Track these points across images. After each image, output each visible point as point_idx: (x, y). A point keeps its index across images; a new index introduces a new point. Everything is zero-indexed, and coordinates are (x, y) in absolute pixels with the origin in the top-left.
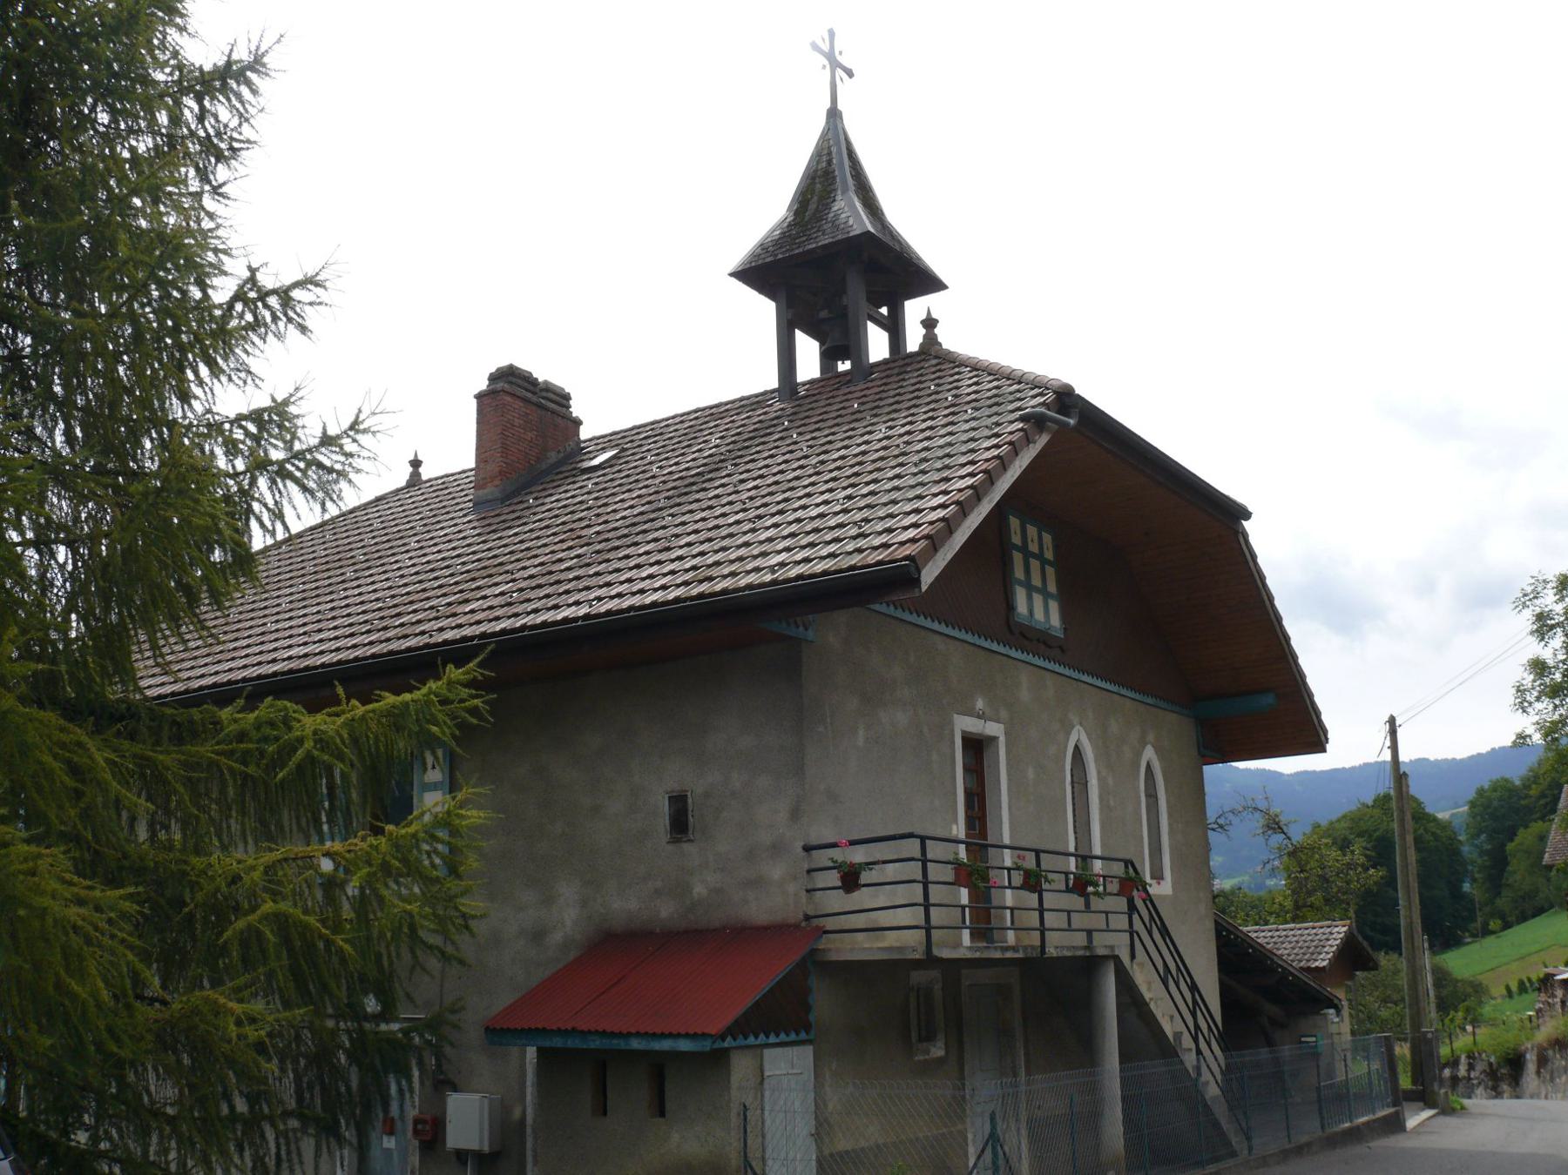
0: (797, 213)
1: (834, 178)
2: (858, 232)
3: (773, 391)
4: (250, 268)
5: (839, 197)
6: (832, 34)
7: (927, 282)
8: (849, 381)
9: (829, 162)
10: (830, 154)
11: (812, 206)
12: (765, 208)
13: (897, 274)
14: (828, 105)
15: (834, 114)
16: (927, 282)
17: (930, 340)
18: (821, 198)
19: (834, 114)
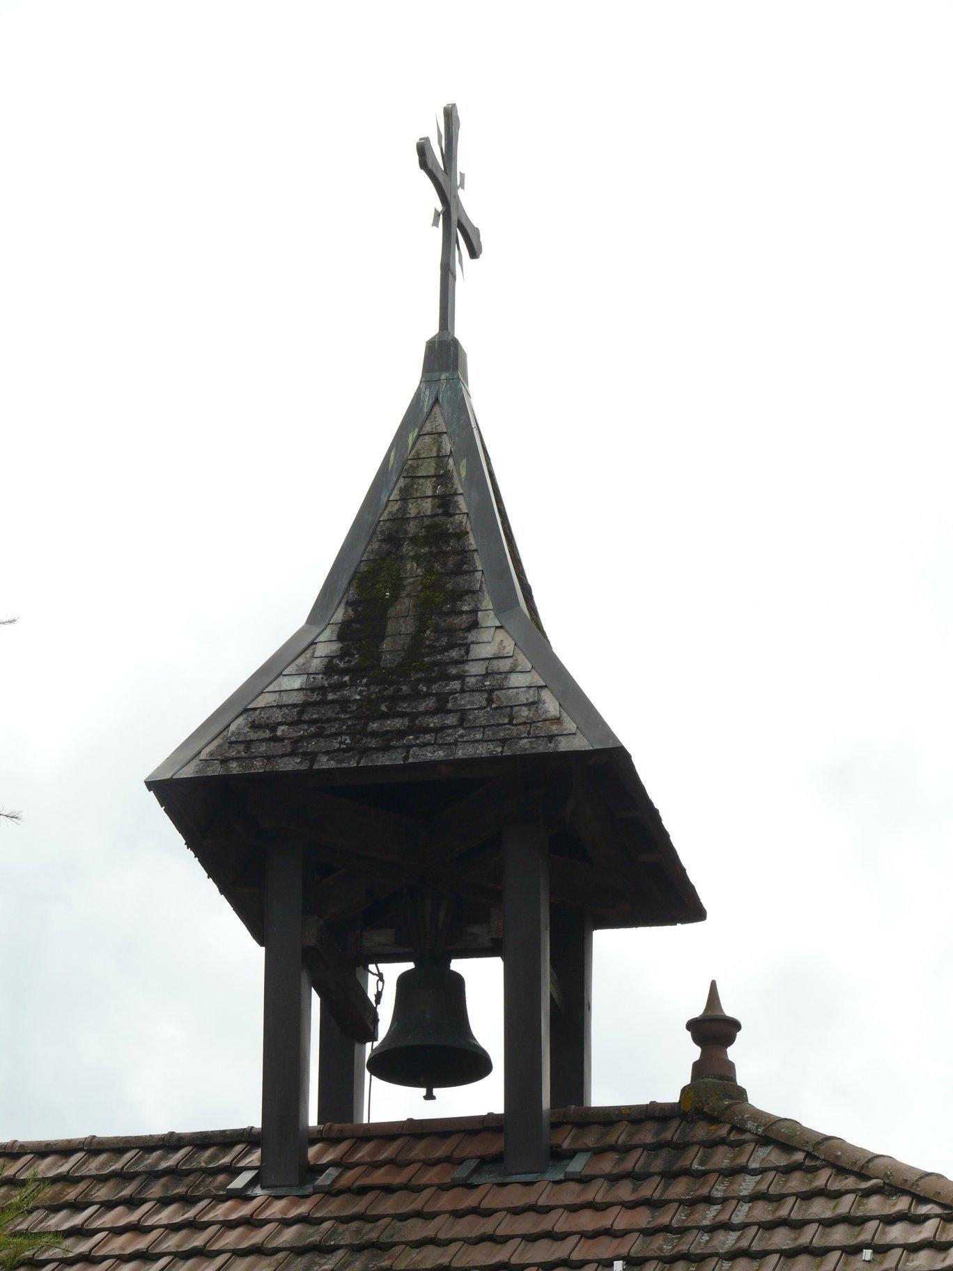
0: (345, 633)
1: (465, 555)
2: (580, 743)
3: (246, 1138)
4: (434, 1098)
5: (489, 619)
6: (450, 115)
7: (665, 895)
8: (495, 1160)
9: (445, 503)
10: (443, 477)
11: (401, 625)
12: (242, 597)
13: (594, 846)
14: (433, 329)
15: (444, 357)
16: (665, 895)
17: (714, 1083)
18: (427, 610)
19: (444, 357)
